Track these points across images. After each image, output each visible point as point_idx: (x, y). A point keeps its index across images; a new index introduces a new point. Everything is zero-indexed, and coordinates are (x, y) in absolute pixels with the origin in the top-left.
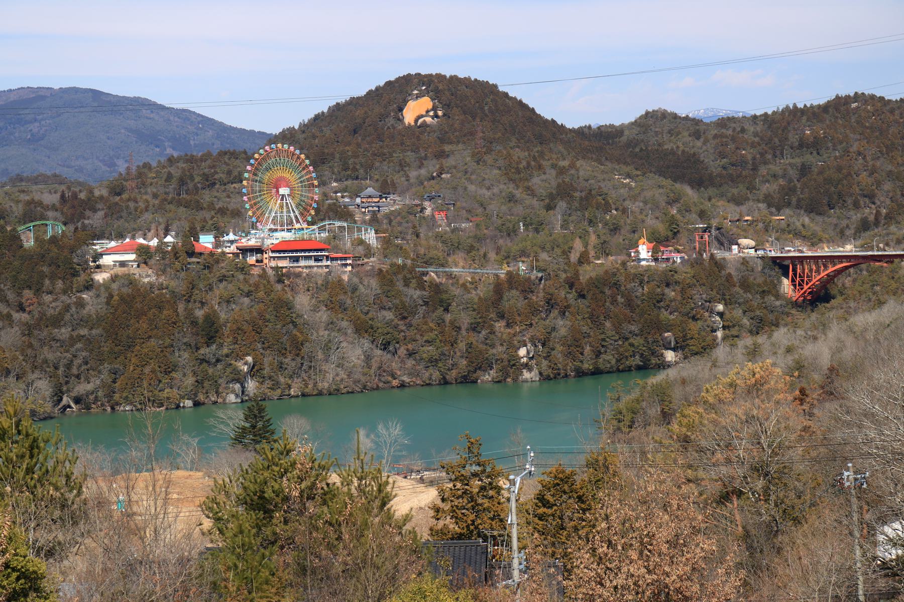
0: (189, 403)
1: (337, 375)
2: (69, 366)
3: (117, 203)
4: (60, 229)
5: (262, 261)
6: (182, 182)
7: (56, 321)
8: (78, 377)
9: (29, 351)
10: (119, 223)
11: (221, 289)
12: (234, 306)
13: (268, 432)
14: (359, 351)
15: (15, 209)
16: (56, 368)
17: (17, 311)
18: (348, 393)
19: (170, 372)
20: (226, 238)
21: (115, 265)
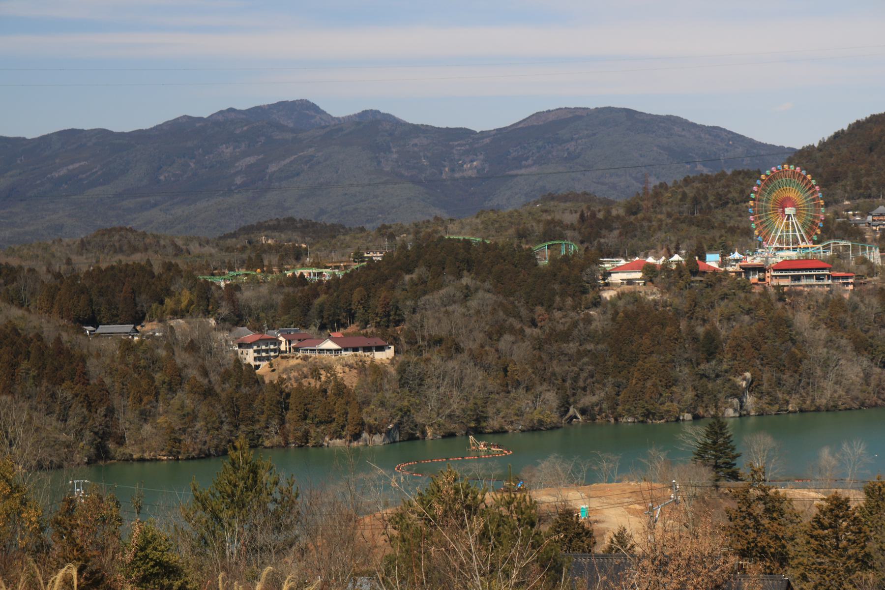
0: (688, 416)
1: (835, 392)
2: (575, 379)
3: (631, 223)
4: (574, 247)
5: (764, 280)
6: (696, 201)
7: (566, 336)
8: (584, 389)
9: (539, 365)
10: (633, 242)
11: (722, 307)
12: (734, 324)
13: (728, 448)
14: (857, 369)
15: (536, 228)
16: (564, 381)
17: (530, 327)
18: (846, 409)
19: (670, 386)
20: (732, 257)
21: (622, 283)
